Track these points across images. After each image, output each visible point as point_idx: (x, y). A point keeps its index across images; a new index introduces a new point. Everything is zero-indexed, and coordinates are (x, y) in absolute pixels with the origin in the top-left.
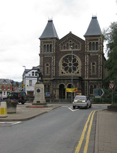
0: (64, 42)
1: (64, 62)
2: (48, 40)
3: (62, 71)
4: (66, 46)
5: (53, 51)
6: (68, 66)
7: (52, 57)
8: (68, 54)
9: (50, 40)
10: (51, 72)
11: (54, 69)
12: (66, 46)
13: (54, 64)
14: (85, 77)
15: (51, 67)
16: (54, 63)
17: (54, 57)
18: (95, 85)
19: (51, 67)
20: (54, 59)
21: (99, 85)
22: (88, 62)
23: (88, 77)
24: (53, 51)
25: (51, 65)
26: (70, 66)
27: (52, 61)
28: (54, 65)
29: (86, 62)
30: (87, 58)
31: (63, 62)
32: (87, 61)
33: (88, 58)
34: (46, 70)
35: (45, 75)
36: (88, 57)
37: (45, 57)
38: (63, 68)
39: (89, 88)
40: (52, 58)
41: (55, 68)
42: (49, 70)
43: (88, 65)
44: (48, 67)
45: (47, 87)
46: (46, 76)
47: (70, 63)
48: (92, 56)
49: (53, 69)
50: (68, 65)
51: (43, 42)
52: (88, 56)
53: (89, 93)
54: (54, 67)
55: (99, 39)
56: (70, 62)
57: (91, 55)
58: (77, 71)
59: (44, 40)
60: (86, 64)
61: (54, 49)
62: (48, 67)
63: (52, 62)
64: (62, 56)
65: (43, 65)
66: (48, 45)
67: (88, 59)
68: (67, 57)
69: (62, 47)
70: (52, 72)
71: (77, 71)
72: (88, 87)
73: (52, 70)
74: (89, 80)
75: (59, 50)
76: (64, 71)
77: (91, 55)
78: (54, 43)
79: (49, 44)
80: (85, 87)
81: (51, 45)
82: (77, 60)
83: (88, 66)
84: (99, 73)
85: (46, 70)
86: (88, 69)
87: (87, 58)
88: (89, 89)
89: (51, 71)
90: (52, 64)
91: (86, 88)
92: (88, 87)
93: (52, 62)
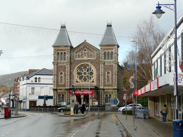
0: (79, 50)
1: (79, 71)
2: (62, 48)
3: (76, 80)
5: (68, 60)
6: (83, 74)
7: (67, 66)
9: (65, 48)
10: (65, 81)
13: (68, 73)
14: (101, 86)
15: (65, 76)
18: (110, 95)
19: (65, 76)
21: (114, 94)
22: (103, 71)
23: (103, 86)
24: (68, 60)
26: (85, 75)
27: (67, 69)
30: (102, 68)
31: (78, 71)
37: (59, 66)
38: (78, 77)
39: (104, 97)
40: (67, 67)
42: (63, 79)
44: (62, 75)
45: (61, 96)
48: (107, 65)
53: (105, 102)
56: (85, 70)
58: (92, 80)
59: (57, 48)
60: (101, 74)
62: (62, 75)
63: (67, 71)
65: (57, 73)
66: (61, 53)
68: (82, 65)
70: (67, 81)
71: (92, 80)
72: (103, 96)
74: (104, 89)
76: (78, 80)
79: (63, 52)
80: (100, 96)
81: (65, 53)
84: (114, 82)
87: (102, 68)
88: (104, 98)
89: (65, 79)
90: (67, 73)
91: (102, 97)
92: (103, 96)
93: (67, 71)
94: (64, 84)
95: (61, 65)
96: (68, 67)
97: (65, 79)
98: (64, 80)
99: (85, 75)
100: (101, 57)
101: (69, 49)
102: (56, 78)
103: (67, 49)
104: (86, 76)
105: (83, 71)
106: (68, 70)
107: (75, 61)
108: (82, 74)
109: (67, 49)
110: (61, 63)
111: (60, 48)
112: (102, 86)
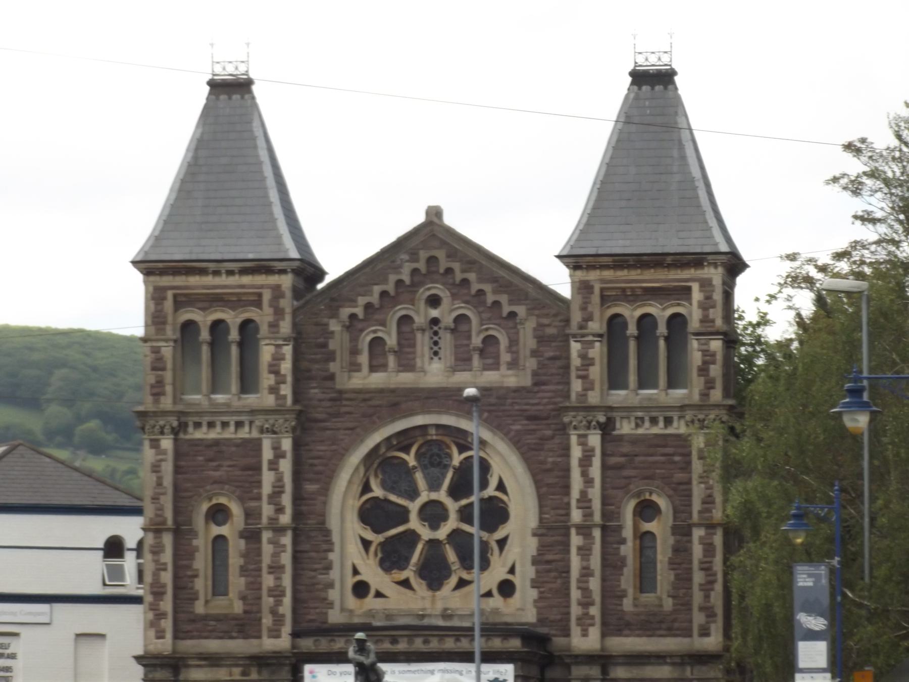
1: (378, 492)
4: (391, 340)
5: (274, 390)
6: (414, 523)
8: (412, 413)
9: (246, 280)
10: (255, 586)
11: (286, 559)
12: (391, 340)
13: (280, 510)
14: (575, 631)
15: (251, 536)
16: (286, 500)
17: (287, 444)
20: (286, 466)
22: (595, 493)
23: (595, 633)
24: (274, 390)
25: (251, 515)
26: (434, 527)
27: (268, 478)
28: (286, 519)
29: (584, 494)
31: (366, 488)
32: (588, 481)
33: (597, 462)
34: (202, 562)
35: (199, 608)
36: (598, 452)
38: (366, 544)
40: (267, 454)
41: (295, 542)
42: (235, 561)
43: (597, 518)
44: (224, 530)
46: (205, 618)
47: (434, 496)
48: (635, 440)
49: (276, 555)
50: (413, 516)
51: (170, 294)
52: (595, 440)
54: (287, 540)
55: (695, 287)
56: (434, 486)
57: (625, 428)
58: (497, 573)
61: (286, 367)
62: (224, 530)
63: (267, 489)
64: (358, 434)
65: (177, 511)
67: (596, 471)
68: (403, 440)
69: (355, 352)
70: (268, 581)
73: (266, 560)
75: (332, 377)
76: (372, 573)
77: (625, 428)
78: (279, 312)
79: (233, 318)
81: (247, 326)
82: (498, 470)
83: (597, 533)
84: (697, 597)
85: (202, 562)
86: (596, 562)
87: (585, 462)
89: (251, 569)
90: (267, 510)
93: (267, 489)
94: (238, 608)
95: (213, 435)
96: (279, 454)
97: (251, 569)
98: (243, 570)
99: (434, 527)
100: (576, 361)
101: (289, 294)
102: (167, 557)
103: (267, 296)
104: (442, 533)
105: (413, 494)
106: (280, 479)
107: (340, 396)
108: (402, 515)
109: (267, 296)
110: (232, 420)
111: (209, 280)
112: (585, 634)
